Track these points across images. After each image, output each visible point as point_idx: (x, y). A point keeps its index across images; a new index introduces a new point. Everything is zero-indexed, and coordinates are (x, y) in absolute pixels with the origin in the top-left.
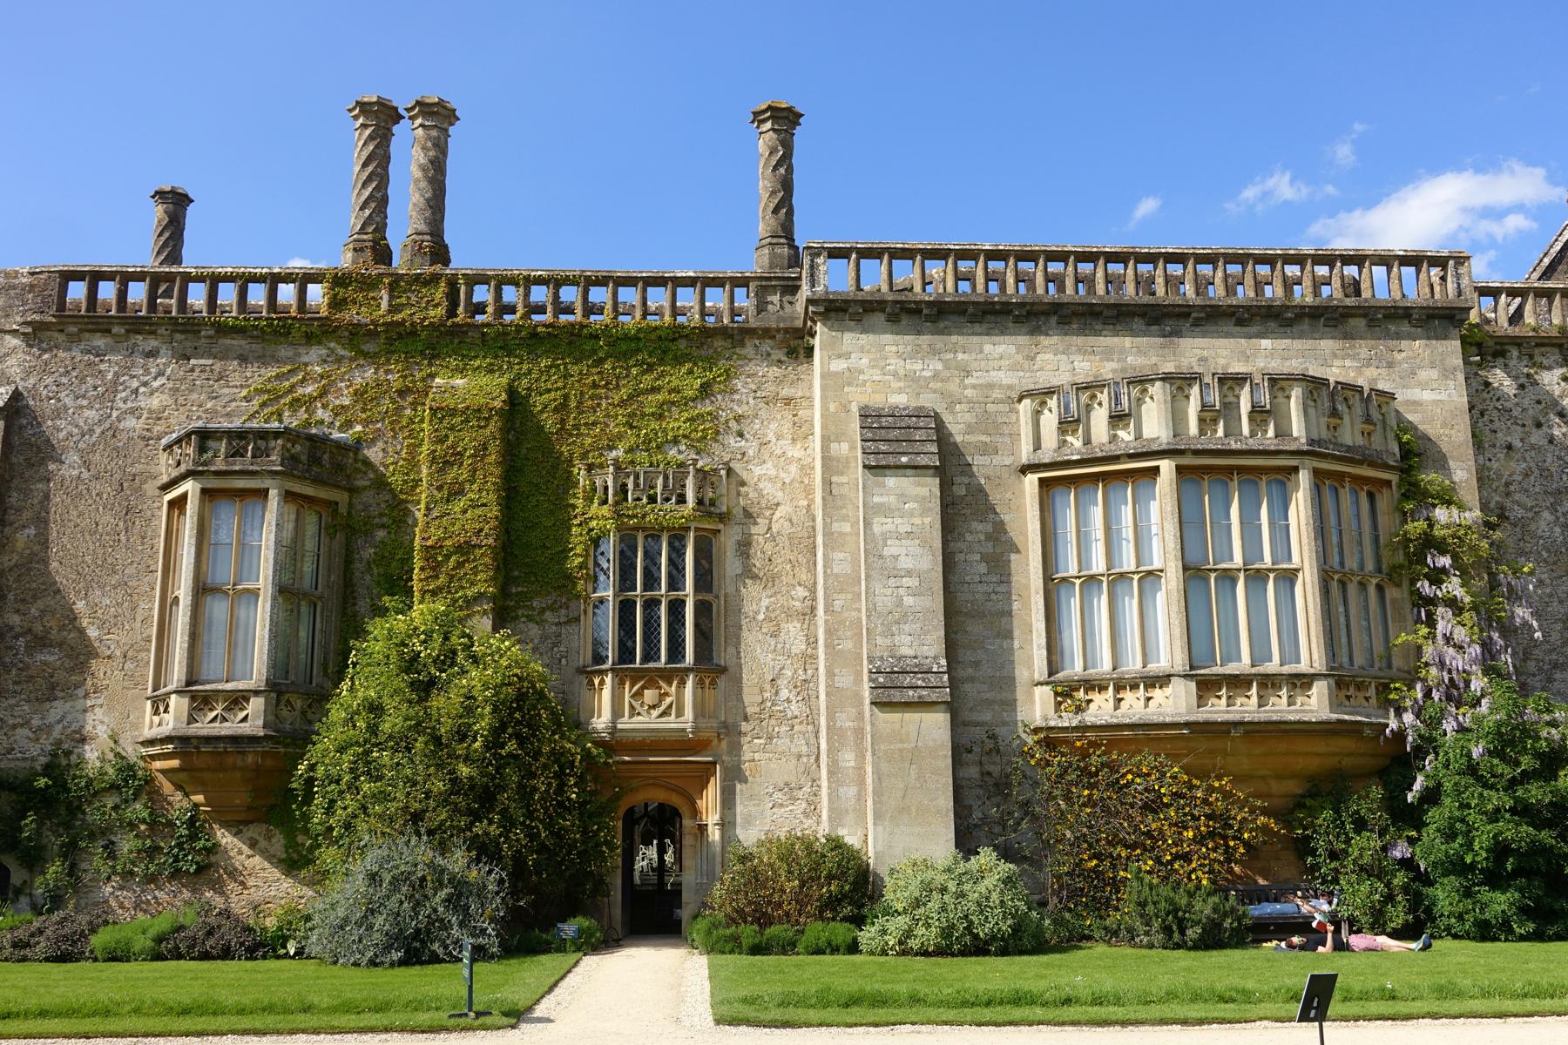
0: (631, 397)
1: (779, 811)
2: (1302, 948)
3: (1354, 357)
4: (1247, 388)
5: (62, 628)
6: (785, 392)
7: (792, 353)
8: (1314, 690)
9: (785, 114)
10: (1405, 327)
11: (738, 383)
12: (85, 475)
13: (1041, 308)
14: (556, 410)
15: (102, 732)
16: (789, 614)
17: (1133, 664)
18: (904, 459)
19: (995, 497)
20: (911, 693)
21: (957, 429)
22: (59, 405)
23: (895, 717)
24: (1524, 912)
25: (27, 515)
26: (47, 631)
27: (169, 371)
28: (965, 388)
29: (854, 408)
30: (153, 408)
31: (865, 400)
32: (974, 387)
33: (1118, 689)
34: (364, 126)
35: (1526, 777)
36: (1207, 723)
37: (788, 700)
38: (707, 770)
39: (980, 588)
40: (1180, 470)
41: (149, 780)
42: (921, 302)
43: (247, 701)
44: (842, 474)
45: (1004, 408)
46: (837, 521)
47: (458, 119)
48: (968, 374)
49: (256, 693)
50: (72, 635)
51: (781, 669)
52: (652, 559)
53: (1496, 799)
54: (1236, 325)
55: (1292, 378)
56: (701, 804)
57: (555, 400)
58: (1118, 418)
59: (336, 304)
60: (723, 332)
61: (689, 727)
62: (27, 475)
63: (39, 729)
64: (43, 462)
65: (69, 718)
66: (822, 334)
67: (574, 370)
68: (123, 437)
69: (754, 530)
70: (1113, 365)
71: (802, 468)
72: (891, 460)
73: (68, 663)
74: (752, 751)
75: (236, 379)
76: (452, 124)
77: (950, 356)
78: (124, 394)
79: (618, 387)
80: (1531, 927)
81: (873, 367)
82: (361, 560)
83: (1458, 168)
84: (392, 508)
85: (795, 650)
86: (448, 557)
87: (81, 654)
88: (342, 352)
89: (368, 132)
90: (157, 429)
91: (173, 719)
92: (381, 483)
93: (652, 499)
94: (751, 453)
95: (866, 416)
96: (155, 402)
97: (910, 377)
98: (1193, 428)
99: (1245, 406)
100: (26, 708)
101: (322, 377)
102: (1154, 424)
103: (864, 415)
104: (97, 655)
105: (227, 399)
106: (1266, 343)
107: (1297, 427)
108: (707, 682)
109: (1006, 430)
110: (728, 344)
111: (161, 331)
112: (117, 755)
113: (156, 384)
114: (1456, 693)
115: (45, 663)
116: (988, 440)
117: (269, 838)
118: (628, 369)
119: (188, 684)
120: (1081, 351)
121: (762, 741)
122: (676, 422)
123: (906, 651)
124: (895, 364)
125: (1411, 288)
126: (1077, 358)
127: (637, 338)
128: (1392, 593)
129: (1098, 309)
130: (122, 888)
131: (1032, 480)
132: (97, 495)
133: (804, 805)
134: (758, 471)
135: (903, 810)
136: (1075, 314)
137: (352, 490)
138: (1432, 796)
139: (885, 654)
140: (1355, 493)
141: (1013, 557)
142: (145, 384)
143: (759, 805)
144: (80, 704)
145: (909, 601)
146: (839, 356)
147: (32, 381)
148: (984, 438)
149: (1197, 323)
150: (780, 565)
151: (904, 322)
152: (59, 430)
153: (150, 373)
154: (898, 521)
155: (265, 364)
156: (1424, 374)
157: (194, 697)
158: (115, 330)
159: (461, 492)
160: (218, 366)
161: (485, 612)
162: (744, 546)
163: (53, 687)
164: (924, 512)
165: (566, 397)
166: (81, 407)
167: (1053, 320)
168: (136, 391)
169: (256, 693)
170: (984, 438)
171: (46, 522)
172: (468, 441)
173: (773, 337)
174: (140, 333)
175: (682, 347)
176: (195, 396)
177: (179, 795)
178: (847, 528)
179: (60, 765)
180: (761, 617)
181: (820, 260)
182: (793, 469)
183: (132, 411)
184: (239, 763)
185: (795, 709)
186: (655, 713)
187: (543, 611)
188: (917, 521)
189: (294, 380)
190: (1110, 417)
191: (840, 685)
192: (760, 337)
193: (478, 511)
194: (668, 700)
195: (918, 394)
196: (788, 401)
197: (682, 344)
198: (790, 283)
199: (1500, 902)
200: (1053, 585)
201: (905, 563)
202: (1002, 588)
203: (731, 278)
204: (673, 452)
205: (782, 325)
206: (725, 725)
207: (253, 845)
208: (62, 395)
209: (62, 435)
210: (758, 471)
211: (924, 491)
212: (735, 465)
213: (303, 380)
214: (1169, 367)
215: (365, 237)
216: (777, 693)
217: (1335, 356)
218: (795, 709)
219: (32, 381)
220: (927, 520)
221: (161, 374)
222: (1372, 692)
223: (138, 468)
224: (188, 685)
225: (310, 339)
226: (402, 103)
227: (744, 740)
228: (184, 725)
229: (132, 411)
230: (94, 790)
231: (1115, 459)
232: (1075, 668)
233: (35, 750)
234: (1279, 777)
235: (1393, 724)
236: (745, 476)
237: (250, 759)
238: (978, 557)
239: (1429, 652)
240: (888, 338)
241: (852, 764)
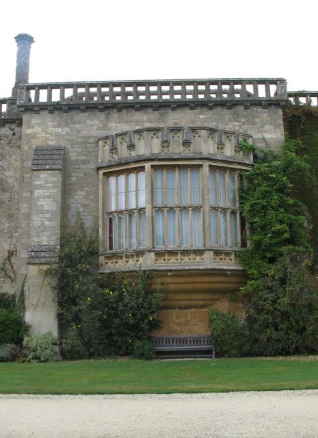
28: (78, 138)
32: (81, 137)
54: (190, 109)
66: (25, 117)
72: (43, 167)
76: (31, 43)
81: (42, 131)
97: (57, 135)
119: (154, 247)
124: (51, 129)
148: (85, 158)
149: (174, 109)
156: (267, 127)
167: (115, 110)
170: (85, 158)
180: (5, 231)
188: (52, 191)
201: (46, 208)
211: (55, 179)
217: (230, 121)
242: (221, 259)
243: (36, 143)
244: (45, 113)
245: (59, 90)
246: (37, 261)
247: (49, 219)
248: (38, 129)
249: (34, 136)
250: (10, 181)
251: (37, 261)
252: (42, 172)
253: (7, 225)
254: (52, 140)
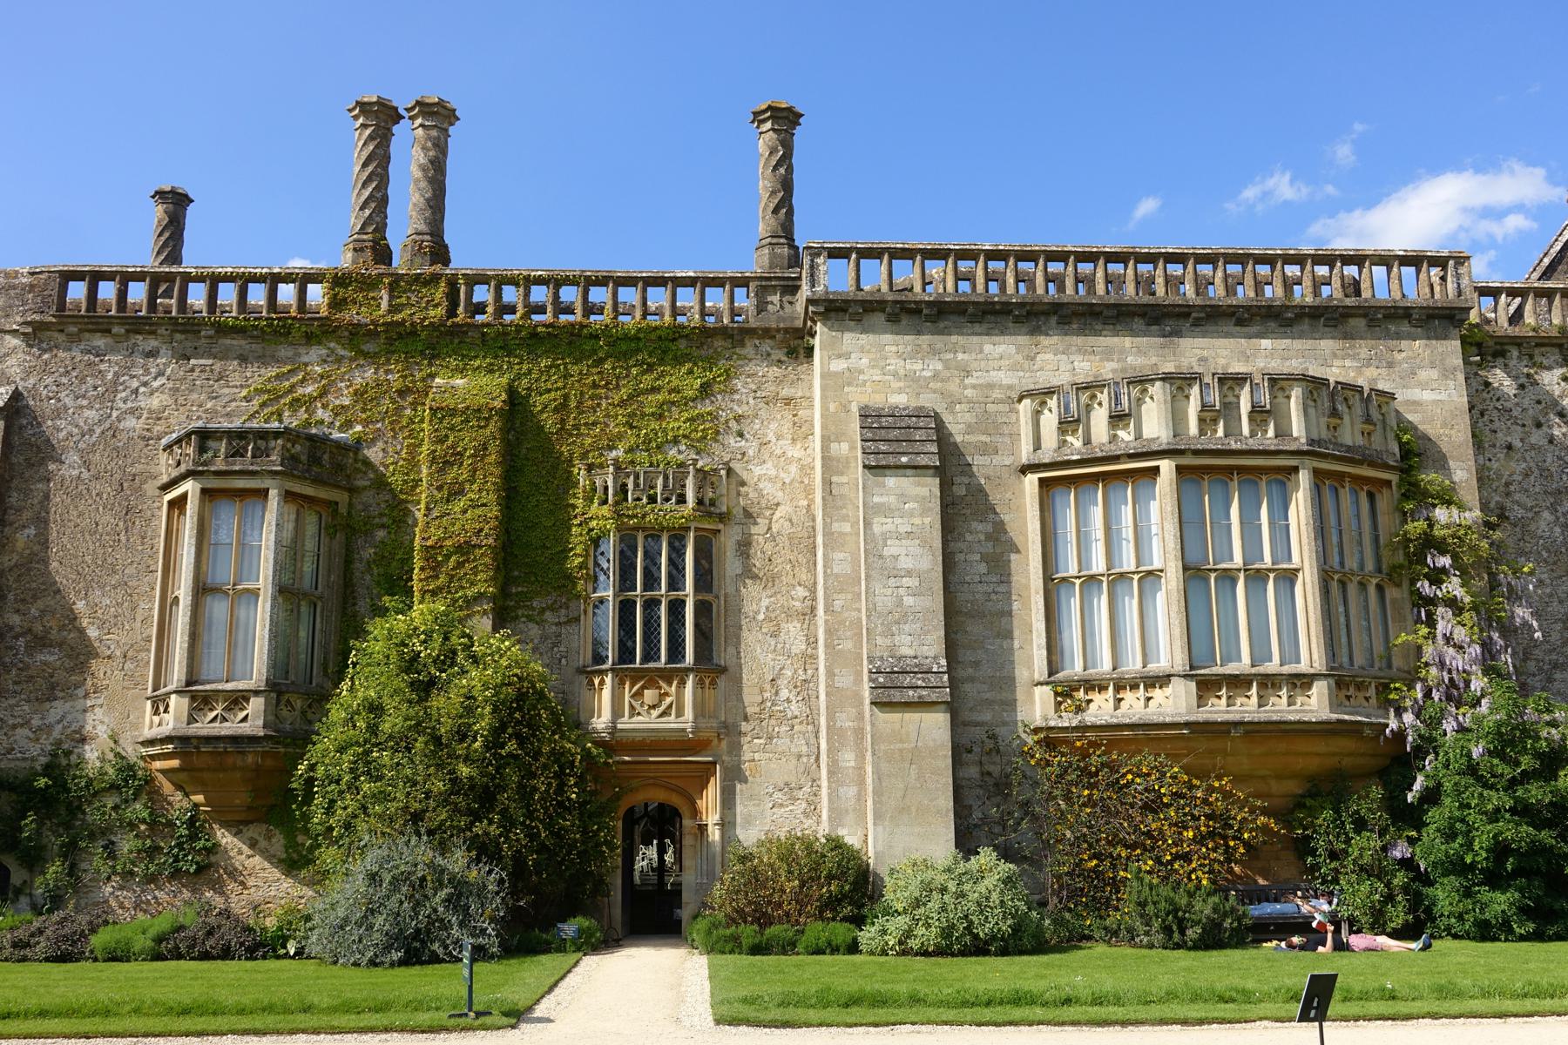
0: (631, 397)
1: (779, 811)
2: (1302, 948)
3: (1354, 357)
4: (1247, 388)
5: (62, 628)
6: (785, 392)
7: (792, 353)
8: (1314, 690)
9: (785, 114)
10: (1405, 327)
11: (738, 383)
12: (85, 475)
13: (1041, 308)
14: (556, 410)
15: (102, 732)
16: (789, 614)
17: (1133, 664)
18: (904, 459)
19: (995, 497)
20: (911, 693)
21: (957, 429)
22: (59, 405)
23: (895, 717)
24: (1524, 912)
25: (27, 515)
26: (47, 631)
27: (169, 371)
28: (965, 388)
29: (854, 408)
30: (153, 408)
31: (865, 400)
32: (974, 387)
33: (1118, 689)
34: (364, 126)
35: (1526, 777)
36: (1207, 723)
37: (788, 700)
38: (707, 770)
39: (980, 588)
40: (1180, 470)
41: (149, 780)
42: (921, 302)
43: (247, 701)
44: (842, 474)
45: (1004, 408)
46: (837, 521)
48: (968, 374)
49: (256, 693)
50: (72, 635)
51: (781, 669)
52: (652, 559)
53: (1496, 799)
54: (1236, 325)
55: (1292, 378)
56: (701, 804)
57: (555, 400)
58: (1118, 418)
59: (336, 304)
60: (723, 332)
61: (689, 727)
62: (27, 475)
63: (39, 729)
64: (43, 462)
65: (69, 718)
66: (822, 334)
67: (574, 370)
68: (123, 437)
69: (754, 530)
70: (1113, 365)
71: (802, 468)
72: (891, 460)
73: (68, 663)
74: (752, 751)
75: (236, 379)
76: (452, 124)
77: (950, 356)
78: (124, 394)
79: (618, 387)
80: (1531, 927)
81: (873, 367)
82: (361, 560)
83: (1458, 168)
84: (392, 508)
85: (795, 650)
86: (448, 557)
87: (81, 654)
88: (342, 352)
89: (368, 132)
90: (157, 429)
91: (173, 719)
92: (381, 483)
93: (652, 499)
94: (751, 453)
95: (866, 416)
96: (155, 402)
97: (910, 377)
98: (1193, 428)
99: (1245, 406)
100: (26, 708)
101: (322, 377)
102: (1154, 424)
103: (864, 415)
104: (97, 655)
105: (227, 399)
106: (1266, 343)
107: (1297, 427)
108: (707, 682)
109: (1006, 430)
110: (728, 344)
111: (161, 331)
112: (117, 755)
113: (156, 384)
114: (1456, 693)
115: (45, 663)
116: (988, 440)
117: (269, 838)
118: (628, 369)
120: (1081, 351)
121: (762, 741)
122: (676, 422)
123: (906, 651)
124: (895, 364)
125: (1411, 288)
126: (1077, 358)
127: (637, 338)
128: (1392, 593)
129: (1098, 309)
130: (122, 888)
131: (1032, 480)
132: (97, 495)
133: (804, 805)
134: (758, 471)
135: (903, 810)
136: (1075, 314)
137: (352, 490)
138: (1432, 796)
139: (885, 654)
140: (1355, 493)
141: (1013, 557)
142: (145, 384)
143: (759, 805)
144: (80, 704)
145: (909, 601)
146: (839, 356)
147: (32, 381)
148: (984, 438)
150: (780, 565)
151: (904, 322)
152: (59, 430)
153: (150, 373)
154: (898, 521)
155: (265, 364)
157: (194, 697)
158: (115, 330)
159: (461, 492)
160: (218, 366)
162: (744, 546)
163: (53, 687)
164: (924, 512)
165: (566, 397)
166: (81, 407)
168: (136, 391)
169: (256, 693)
170: (984, 438)
171: (46, 522)
172: (468, 441)
173: (773, 337)
174: (140, 333)
175: (682, 347)
176: (195, 396)
177: (179, 795)
178: (847, 528)
179: (60, 765)
180: (761, 617)
181: (820, 260)
182: (793, 469)
183: (132, 411)
184: (239, 763)
185: (795, 709)
186: (655, 713)
187: (543, 611)
188: (917, 521)
189: (294, 380)
190: (1110, 417)
191: (840, 685)
192: (760, 337)
193: (478, 511)
194: (668, 700)
195: (918, 394)
196: (788, 401)
197: (682, 344)
198: (790, 283)
199: (1500, 902)
200: (1053, 585)
201: (905, 563)
202: (1002, 588)
203: (731, 278)
204: (673, 452)
205: (782, 325)
206: (725, 725)
207: (253, 845)
208: (62, 395)
209: (62, 435)
210: (758, 471)
211: (924, 491)
212: (735, 465)
213: (303, 380)
214: (1169, 367)
215: (365, 237)
216: (777, 693)
217: (1335, 356)
218: (795, 709)
219: (32, 381)
220: (927, 520)
221: (161, 374)
222: (1372, 692)
223: (138, 468)
224: (188, 685)
225: (310, 339)
226: (402, 103)
227: (744, 740)
228: (184, 725)
229: (132, 411)
230: (94, 790)
231: (1115, 459)
232: (1075, 668)
233: (35, 750)
234: (1279, 777)
235: (1393, 724)
236: (745, 476)
237: (250, 759)
238: (978, 557)
239: (1429, 652)
240: (888, 338)
241: (852, 764)
242: (1348, 698)
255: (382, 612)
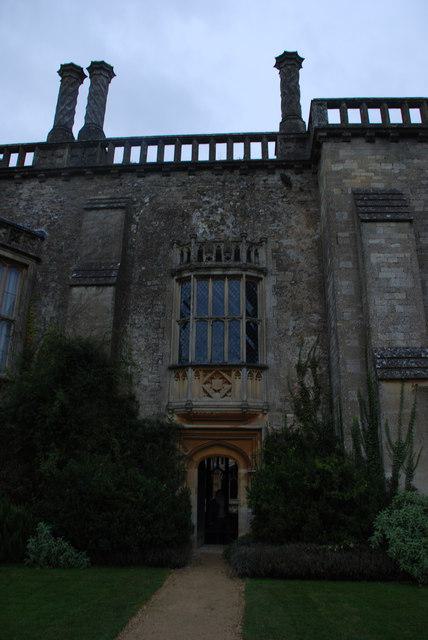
47: (303, 59)
97: (384, 173)
103: (354, 193)
108: (255, 374)
124: (374, 166)
151: (377, 142)
161: (355, 338)
180: (290, 333)
201: (396, 283)
211: (403, 236)
226: (85, 64)
243: (351, 184)
244: (360, 143)
245: (208, 145)
246: (397, 374)
247: (405, 303)
248: (350, 165)
249: (347, 174)
250: (292, 253)
251: (397, 374)
252: (378, 224)
253: (292, 323)
254: (378, 181)
255: (385, 543)
